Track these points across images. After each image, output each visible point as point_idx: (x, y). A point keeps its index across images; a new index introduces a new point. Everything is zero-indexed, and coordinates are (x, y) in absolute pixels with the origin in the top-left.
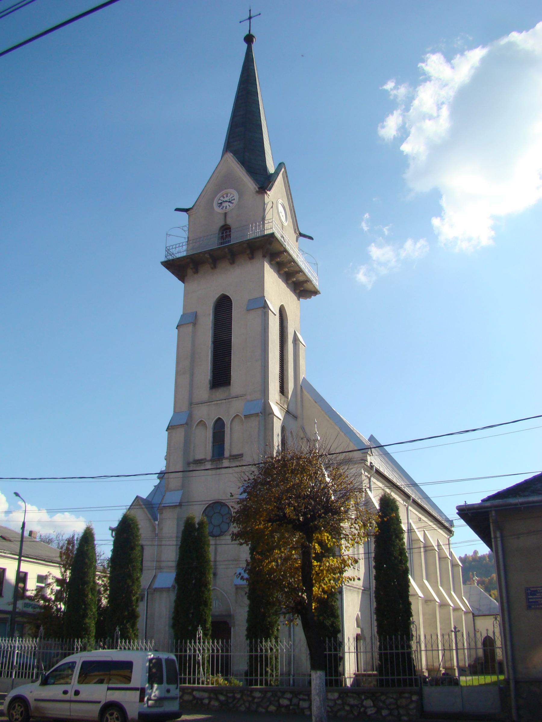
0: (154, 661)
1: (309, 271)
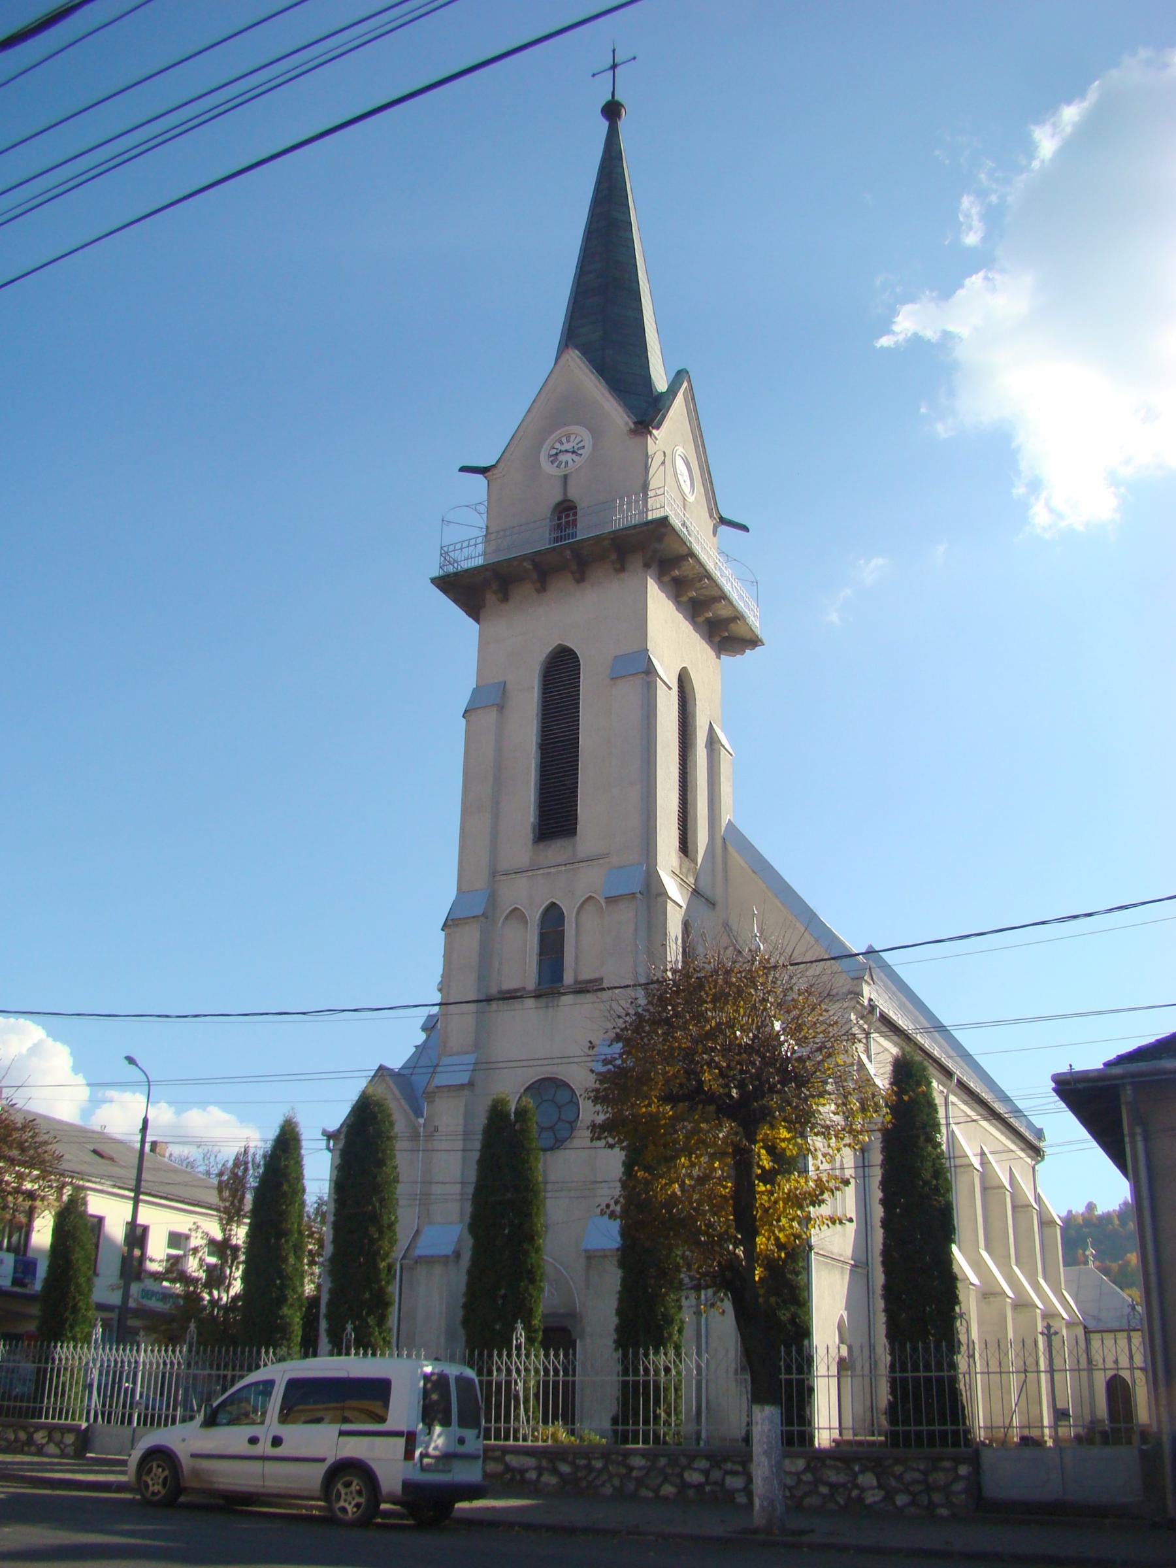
0: (434, 1378)
1: (741, 597)
